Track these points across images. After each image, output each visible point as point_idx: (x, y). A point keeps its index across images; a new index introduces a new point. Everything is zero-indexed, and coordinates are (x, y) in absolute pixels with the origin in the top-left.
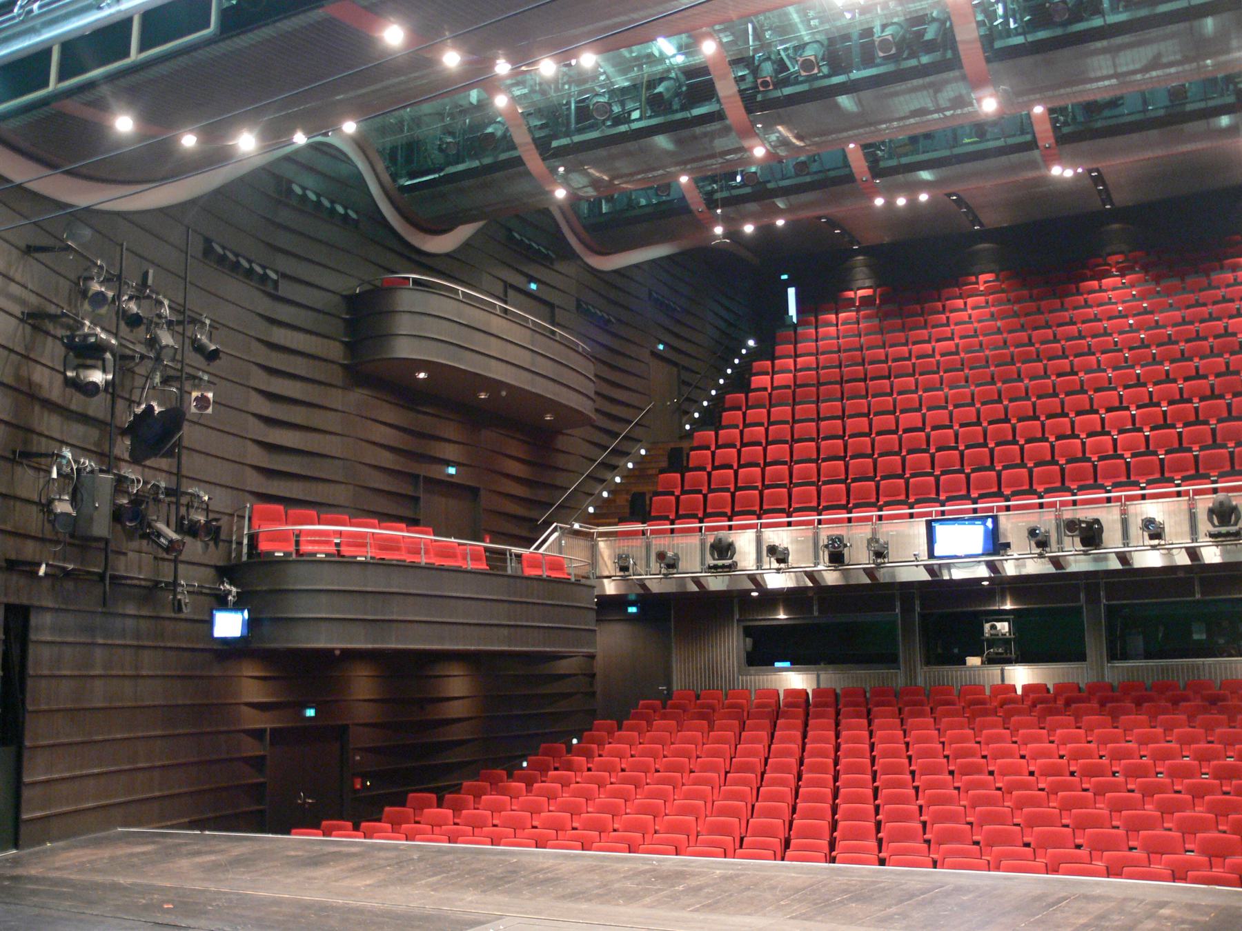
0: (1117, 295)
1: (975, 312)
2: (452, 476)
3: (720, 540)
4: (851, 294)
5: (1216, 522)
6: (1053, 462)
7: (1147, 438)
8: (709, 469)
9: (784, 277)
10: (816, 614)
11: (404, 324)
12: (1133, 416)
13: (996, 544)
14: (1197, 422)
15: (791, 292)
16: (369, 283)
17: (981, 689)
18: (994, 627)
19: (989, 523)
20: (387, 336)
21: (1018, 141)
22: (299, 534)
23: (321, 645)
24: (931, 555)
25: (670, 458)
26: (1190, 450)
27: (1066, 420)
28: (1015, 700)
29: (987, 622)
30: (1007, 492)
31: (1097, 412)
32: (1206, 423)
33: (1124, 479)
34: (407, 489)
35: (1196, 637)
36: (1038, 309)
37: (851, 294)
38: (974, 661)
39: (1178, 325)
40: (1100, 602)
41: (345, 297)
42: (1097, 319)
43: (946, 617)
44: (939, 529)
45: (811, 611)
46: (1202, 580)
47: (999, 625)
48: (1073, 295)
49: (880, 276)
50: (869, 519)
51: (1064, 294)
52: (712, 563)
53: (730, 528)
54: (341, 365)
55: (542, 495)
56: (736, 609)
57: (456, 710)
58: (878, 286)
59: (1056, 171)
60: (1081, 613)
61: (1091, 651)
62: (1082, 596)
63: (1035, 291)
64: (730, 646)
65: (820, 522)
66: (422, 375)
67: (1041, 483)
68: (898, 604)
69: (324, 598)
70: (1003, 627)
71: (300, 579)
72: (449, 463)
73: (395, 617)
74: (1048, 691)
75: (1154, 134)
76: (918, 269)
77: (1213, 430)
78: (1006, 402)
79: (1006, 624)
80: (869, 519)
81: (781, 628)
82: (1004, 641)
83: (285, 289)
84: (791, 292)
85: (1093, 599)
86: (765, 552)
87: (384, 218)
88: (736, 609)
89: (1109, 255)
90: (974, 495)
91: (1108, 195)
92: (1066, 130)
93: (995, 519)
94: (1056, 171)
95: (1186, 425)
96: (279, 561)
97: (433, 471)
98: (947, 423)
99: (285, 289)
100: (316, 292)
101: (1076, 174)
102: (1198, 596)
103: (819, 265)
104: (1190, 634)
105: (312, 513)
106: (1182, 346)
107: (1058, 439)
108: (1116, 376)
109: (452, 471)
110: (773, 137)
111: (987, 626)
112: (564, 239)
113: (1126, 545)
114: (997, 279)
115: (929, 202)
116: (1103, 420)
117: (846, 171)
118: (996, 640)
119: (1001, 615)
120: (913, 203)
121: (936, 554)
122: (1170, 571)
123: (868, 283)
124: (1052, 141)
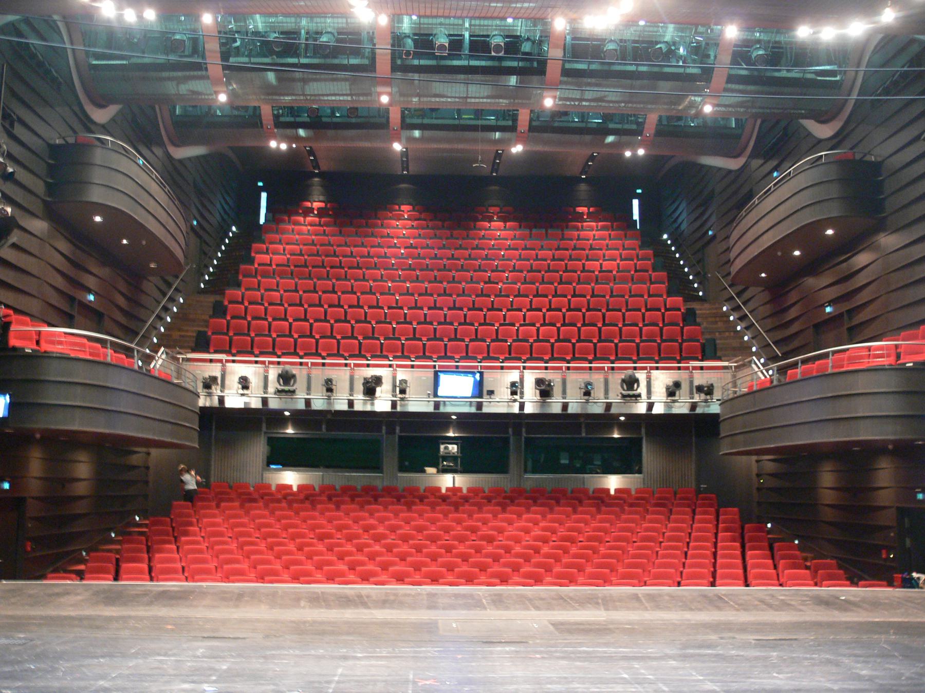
0: (498, 234)
1: (401, 231)
2: (91, 301)
3: (287, 372)
4: (309, 204)
5: (625, 387)
6: (290, 336)
7: (414, 329)
8: (640, 325)
9: (260, 184)
10: (324, 430)
11: (98, 176)
12: (405, 314)
13: (480, 389)
14: (425, 322)
15: (264, 196)
16: (64, 138)
17: (269, 486)
18: (446, 448)
19: (478, 376)
20: (83, 184)
21: (249, 120)
22: (39, 333)
23: (75, 427)
24: (436, 395)
25: (214, 308)
26: (399, 339)
27: (322, 309)
28: (293, 494)
29: (443, 443)
30: (257, 352)
31: (362, 307)
32: (411, 323)
33: (379, 354)
34: (65, 307)
35: (563, 462)
36: (452, 236)
37: (309, 204)
38: (431, 470)
39: (433, 259)
40: (395, 433)
41: (49, 145)
42: (379, 246)
43: (416, 437)
44: (442, 377)
45: (320, 430)
46: (587, 425)
47: (450, 447)
48: (472, 229)
49: (331, 195)
50: (645, 368)
51: (467, 228)
52: (280, 388)
53: (635, 368)
54: (43, 201)
55: (132, 325)
56: (264, 426)
57: (81, 489)
58: (329, 202)
59: (273, 144)
60: (508, 443)
61: (386, 467)
62: (510, 430)
63: (615, 224)
64: (258, 449)
65: (524, 368)
66: (98, 219)
67: (280, 349)
68: (384, 428)
69: (79, 390)
70: (453, 448)
71: (53, 373)
72: (90, 291)
73: (122, 410)
74: (314, 489)
75: (588, 138)
76: (359, 195)
77: (476, 330)
78: (301, 293)
79: (455, 446)
80: (560, 368)
81: (289, 440)
82: (453, 458)
83: (18, 130)
84: (264, 196)
85: (518, 433)
86: (695, 390)
87: (74, 86)
88: (264, 426)
89: (491, 206)
90: (234, 351)
91: (317, 163)
92: (534, 124)
93: (481, 374)
94: (273, 144)
95: (398, 323)
96: (29, 356)
97: (79, 294)
98: (240, 300)
99: (18, 130)
100: (35, 138)
101: (290, 148)
102: (584, 435)
103: (289, 183)
104: (559, 459)
105: (28, 319)
106: (436, 273)
107: (274, 319)
108: (394, 286)
109: (92, 298)
110: (231, 88)
111: (442, 447)
112: (159, 130)
113: (265, 393)
114: (414, 210)
115: (646, 156)
116: (366, 313)
117: (384, 120)
118: (448, 457)
119: (451, 440)
120: (634, 155)
121: (439, 394)
122: (247, 411)
123: (321, 198)
124: (527, 128)
